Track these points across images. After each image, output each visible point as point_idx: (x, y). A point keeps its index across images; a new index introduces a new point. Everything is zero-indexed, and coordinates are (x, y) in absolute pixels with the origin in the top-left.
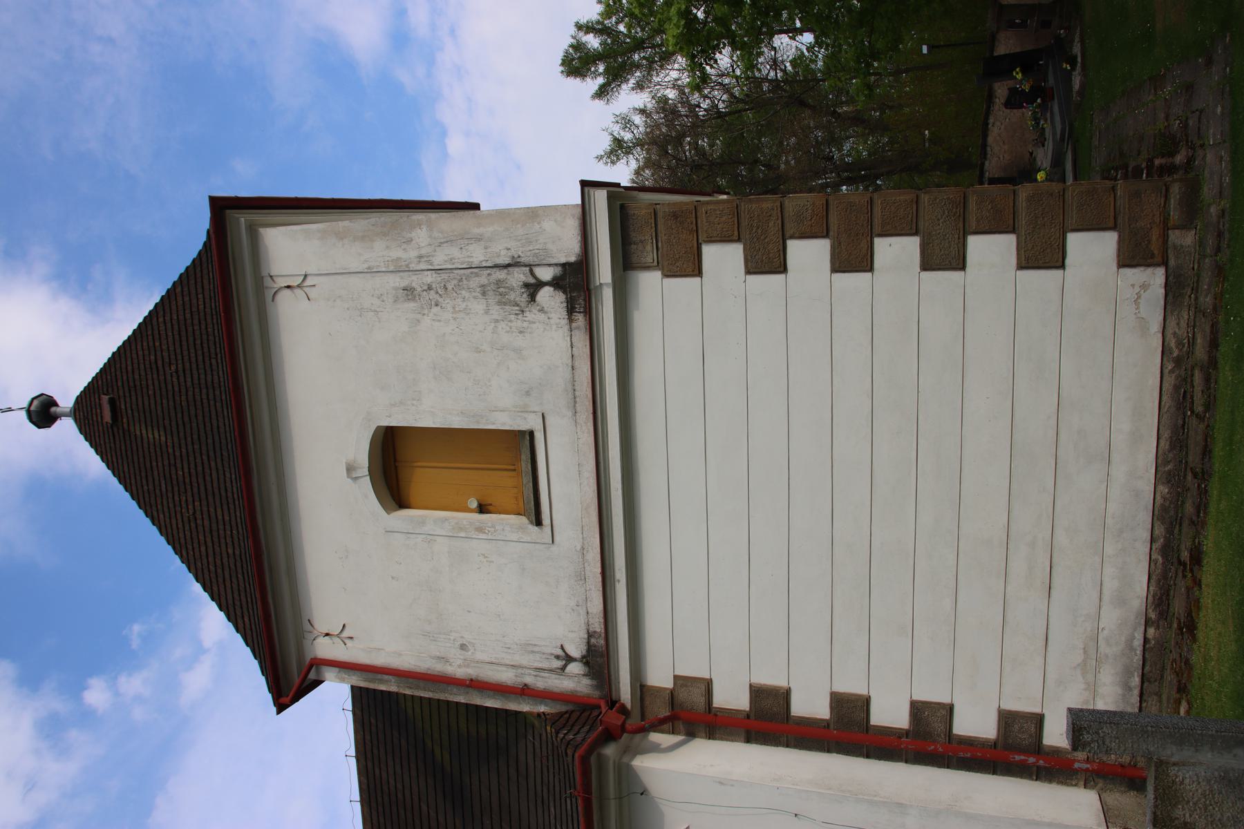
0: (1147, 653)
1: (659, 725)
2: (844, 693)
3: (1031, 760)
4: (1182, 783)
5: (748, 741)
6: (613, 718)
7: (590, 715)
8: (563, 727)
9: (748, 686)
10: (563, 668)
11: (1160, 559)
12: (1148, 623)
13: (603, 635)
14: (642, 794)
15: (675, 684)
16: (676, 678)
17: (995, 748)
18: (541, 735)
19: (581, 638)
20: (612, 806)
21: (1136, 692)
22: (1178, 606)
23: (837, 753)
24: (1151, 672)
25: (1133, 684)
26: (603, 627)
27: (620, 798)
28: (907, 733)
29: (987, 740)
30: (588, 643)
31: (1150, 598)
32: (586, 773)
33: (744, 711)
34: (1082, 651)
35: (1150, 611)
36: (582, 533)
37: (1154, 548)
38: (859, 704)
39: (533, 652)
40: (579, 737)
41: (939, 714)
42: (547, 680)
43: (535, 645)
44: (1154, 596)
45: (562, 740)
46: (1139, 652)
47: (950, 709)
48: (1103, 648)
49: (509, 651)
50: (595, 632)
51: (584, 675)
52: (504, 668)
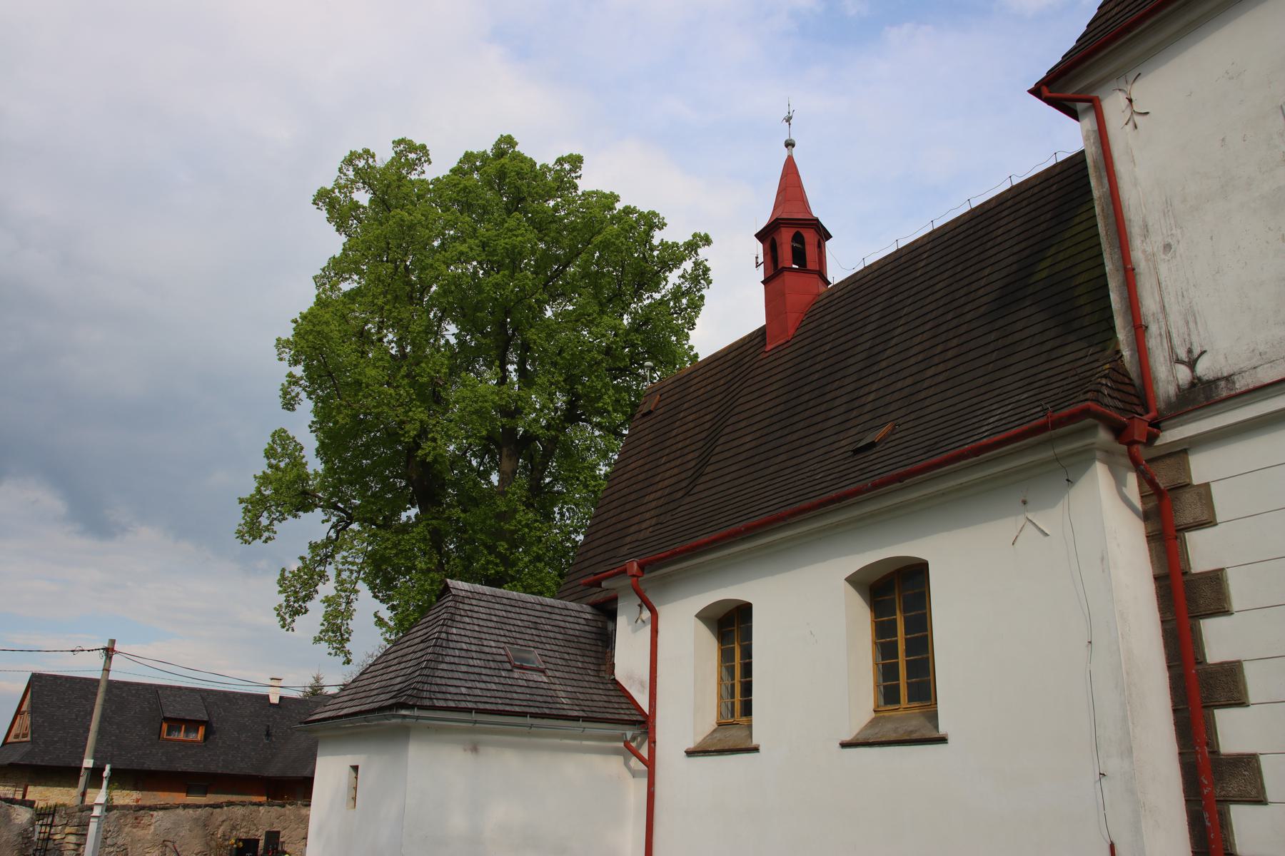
1: (1147, 480)
2: (1244, 676)
5: (1157, 578)
6: (1139, 430)
10: (1179, 361)
13: (1233, 393)
14: (1068, 480)
16: (1207, 486)
18: (1097, 360)
26: (1243, 389)
28: (1215, 752)
32: (1072, 418)
33: (1190, 568)
39: (1187, 323)
40: (1107, 400)
43: (1196, 323)
45: (1099, 383)
49: (1180, 298)
50: (1234, 383)
51: (1178, 386)
52: (1158, 299)
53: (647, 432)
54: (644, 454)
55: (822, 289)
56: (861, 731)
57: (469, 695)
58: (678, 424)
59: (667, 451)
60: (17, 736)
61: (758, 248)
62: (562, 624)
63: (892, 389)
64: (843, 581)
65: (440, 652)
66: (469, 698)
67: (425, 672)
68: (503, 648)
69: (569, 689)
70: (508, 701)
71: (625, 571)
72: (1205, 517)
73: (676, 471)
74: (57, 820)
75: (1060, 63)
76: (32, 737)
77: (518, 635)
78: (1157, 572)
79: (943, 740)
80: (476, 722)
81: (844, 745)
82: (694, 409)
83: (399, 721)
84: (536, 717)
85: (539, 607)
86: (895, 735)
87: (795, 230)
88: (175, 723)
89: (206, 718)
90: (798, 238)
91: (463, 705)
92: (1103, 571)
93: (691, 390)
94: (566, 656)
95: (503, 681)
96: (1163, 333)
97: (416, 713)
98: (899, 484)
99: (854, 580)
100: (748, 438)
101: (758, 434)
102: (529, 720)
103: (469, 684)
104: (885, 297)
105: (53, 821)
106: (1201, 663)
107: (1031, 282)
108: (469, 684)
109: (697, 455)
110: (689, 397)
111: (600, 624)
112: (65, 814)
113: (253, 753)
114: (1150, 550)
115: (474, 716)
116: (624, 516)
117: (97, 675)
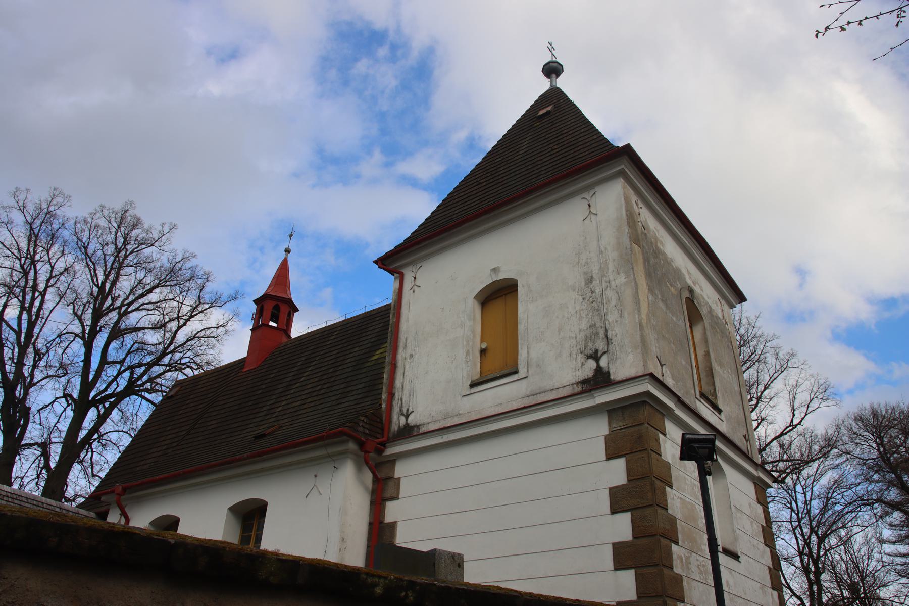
5: (370, 524)
7: (379, 433)
10: (402, 414)
14: (335, 467)
16: (399, 479)
27: (330, 456)
30: (415, 426)
33: (384, 520)
40: (361, 429)
50: (420, 429)
52: (402, 381)
55: (285, 340)
61: (254, 308)
71: (113, 492)
72: (394, 495)
75: (393, 250)
87: (276, 303)
90: (277, 308)
100: (214, 422)
107: (370, 360)
114: (371, 509)
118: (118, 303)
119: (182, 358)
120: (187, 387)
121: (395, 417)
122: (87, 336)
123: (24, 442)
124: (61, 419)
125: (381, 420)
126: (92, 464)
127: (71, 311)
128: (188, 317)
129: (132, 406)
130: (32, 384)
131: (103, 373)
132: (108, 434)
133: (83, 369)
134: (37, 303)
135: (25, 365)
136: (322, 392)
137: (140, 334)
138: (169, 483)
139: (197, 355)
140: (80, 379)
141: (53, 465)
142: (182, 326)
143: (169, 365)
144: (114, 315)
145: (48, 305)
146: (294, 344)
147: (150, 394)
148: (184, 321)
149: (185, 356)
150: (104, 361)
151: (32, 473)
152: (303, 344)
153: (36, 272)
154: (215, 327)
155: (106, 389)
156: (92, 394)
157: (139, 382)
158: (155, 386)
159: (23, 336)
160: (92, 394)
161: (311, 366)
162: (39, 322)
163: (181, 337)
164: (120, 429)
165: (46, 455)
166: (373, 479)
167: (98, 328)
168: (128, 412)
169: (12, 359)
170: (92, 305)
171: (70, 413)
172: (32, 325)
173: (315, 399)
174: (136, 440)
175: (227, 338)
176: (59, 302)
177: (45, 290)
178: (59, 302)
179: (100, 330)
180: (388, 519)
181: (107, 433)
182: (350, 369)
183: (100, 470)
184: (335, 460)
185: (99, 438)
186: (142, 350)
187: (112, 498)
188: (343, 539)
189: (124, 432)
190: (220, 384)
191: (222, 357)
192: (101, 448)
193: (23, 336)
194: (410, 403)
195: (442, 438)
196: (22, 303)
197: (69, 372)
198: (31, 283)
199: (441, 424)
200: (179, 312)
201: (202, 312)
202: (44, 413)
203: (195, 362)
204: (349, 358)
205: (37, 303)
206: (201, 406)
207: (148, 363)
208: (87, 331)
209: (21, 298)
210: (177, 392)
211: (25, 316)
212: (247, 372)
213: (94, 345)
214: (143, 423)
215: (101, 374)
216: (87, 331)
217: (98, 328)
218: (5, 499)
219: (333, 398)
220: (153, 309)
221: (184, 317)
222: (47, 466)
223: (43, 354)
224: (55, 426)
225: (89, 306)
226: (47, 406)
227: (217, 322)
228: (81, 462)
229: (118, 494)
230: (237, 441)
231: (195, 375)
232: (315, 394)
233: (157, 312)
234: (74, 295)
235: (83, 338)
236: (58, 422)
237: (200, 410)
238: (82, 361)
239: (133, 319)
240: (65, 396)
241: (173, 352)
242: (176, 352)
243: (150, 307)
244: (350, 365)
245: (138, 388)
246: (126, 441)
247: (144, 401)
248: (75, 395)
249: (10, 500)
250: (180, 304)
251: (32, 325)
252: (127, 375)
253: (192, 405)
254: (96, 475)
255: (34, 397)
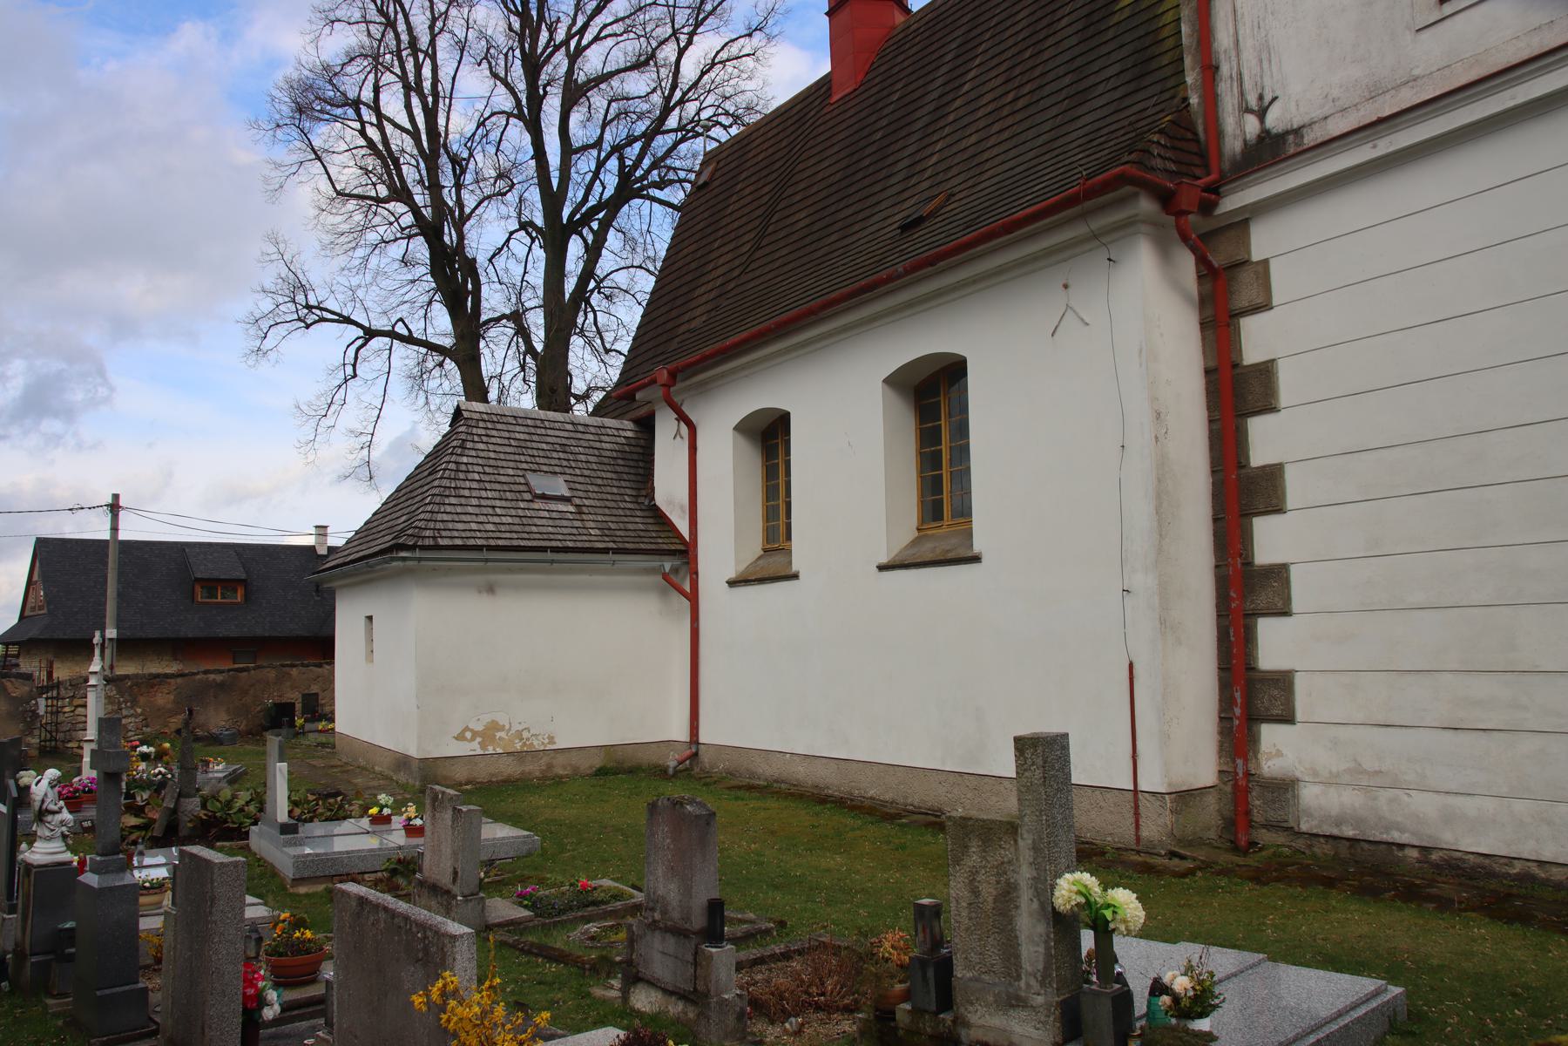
0: (1384, 846)
1: (1202, 261)
2: (1284, 480)
3: (1238, 711)
4: (1000, 846)
5: (1208, 372)
6: (1189, 197)
7: (1196, 166)
8: (1170, 138)
9: (1273, 357)
10: (1248, 110)
11: (1515, 871)
12: (1425, 850)
13: (1300, 149)
14: (1109, 260)
15: (1258, 263)
16: (1265, 262)
17: (1247, 669)
18: (1162, 111)
19: (1291, 120)
20: (1080, 230)
21: (1335, 832)
22: (1446, 889)
23: (1213, 483)
24: (1362, 849)
25: (1344, 828)
26: (1312, 144)
27: (1095, 236)
28: (1249, 563)
29: (1255, 659)
30: (1287, 133)
31: (1458, 855)
32: (1107, 186)
33: (1242, 360)
34: (1377, 769)
35: (1441, 854)
36: (1439, 70)
37: (1529, 864)
38: (1274, 501)
39: (1261, 61)
40: (1158, 163)
41: (1276, 599)
42: (1229, 94)
43: (1270, 61)
44: (1460, 859)
45: (1150, 141)
46: (1385, 837)
47: (1285, 612)
48: (1384, 795)
49: (1256, 29)
50: (1302, 137)
51: (1245, 141)
52: (1231, 31)
53: (701, 209)
54: (696, 237)
55: (900, 18)
56: (901, 552)
57: (479, 531)
58: (734, 198)
59: (721, 233)
60: (33, 609)
62: (598, 445)
63: (955, 149)
64: (878, 386)
65: (448, 485)
66: (479, 534)
67: (429, 508)
68: (523, 476)
69: (599, 518)
70: (526, 536)
71: (654, 382)
73: (729, 256)
74: (63, 692)
76: (48, 610)
77: (542, 461)
78: (1212, 364)
79: (976, 559)
80: (487, 560)
81: (882, 568)
82: (754, 179)
83: (400, 564)
84: (558, 552)
85: (569, 427)
86: (931, 555)
88: (211, 585)
89: (243, 576)
91: (471, 542)
92: (1141, 365)
93: (751, 155)
94: (599, 482)
95: (521, 513)
96: (1234, 75)
97: (418, 554)
98: (930, 269)
99: (892, 381)
100: (803, 214)
101: (812, 210)
102: (549, 555)
103: (482, 519)
104: (963, 30)
105: (58, 694)
106: (1244, 467)
108: (482, 519)
109: (753, 235)
110: (748, 164)
111: (642, 442)
112: (71, 685)
113: (303, 612)
114: (1204, 339)
115: (486, 554)
116: (674, 313)
117: (106, 536)
118: (560, 35)
119: (700, 109)
120: (729, 159)
121: (1229, 121)
122: (526, 110)
123: (484, 318)
124: (529, 267)
125: (1196, 134)
126: (599, 332)
127: (487, 73)
128: (691, 28)
129: (638, 217)
130: (464, 219)
131: (573, 170)
132: (611, 276)
133: (537, 170)
134: (427, 72)
135: (444, 187)
136: (1020, 104)
137: (615, 82)
138: (767, 343)
139: (727, 98)
140: (538, 190)
141: (539, 347)
142: (686, 48)
143: (681, 128)
144: (560, 60)
145: (445, 73)
146: (923, 21)
147: (662, 189)
148: (687, 36)
149: (704, 105)
150: (568, 150)
151: (512, 366)
152: (945, 15)
153: (406, 16)
154: (745, 36)
155: (585, 199)
156: (566, 213)
157: (639, 173)
158: (665, 175)
159: (424, 137)
160: (566, 213)
161: (977, 56)
162: (441, 105)
163: (689, 71)
164: (628, 263)
165: (523, 332)
166: (1198, 271)
167: (541, 92)
168: (633, 231)
169: (421, 182)
170: (517, 53)
171: (539, 253)
172: (431, 114)
173: (1009, 121)
174: (663, 278)
175: (772, 50)
176: (461, 58)
177: (432, 43)
178: (461, 58)
179: (546, 93)
180: (1252, 355)
181: (608, 275)
182: (1074, 40)
183: (616, 339)
184: (1108, 240)
185: (598, 287)
186: (626, 113)
187: (656, 392)
188: (1159, 414)
189: (637, 267)
190: (792, 138)
191: (769, 92)
192: (605, 301)
193: (424, 137)
194: (1265, 79)
195: (1375, 147)
196: (403, 77)
197: (515, 181)
198: (404, 37)
199: (1362, 113)
200: (673, 22)
201: (710, 13)
202: (500, 262)
203: (727, 113)
204: (1063, 17)
205: (427, 72)
206: (766, 189)
207: (644, 135)
208: (524, 102)
209: (397, 70)
210: (713, 174)
211: (415, 101)
212: (840, 103)
213: (543, 125)
214: (666, 246)
215: (570, 174)
216: (524, 102)
217: (541, 92)
218: (481, 424)
219: (1054, 111)
220: (624, 32)
221: (686, 30)
222: (530, 349)
223: (464, 159)
224: (523, 280)
225: (514, 56)
226: (500, 249)
227: (747, 23)
228: (582, 333)
229: (663, 385)
230: (862, 241)
231: (732, 138)
232: (1005, 112)
233: (632, 35)
234: (484, 43)
235: (520, 117)
236: (525, 272)
237: (767, 197)
238: (532, 158)
239: (593, 61)
240: (525, 226)
241: (682, 102)
242: (688, 101)
243: (618, 28)
244: (1070, 30)
245: (639, 185)
246: (646, 283)
247: (656, 206)
248: (539, 221)
249: (489, 425)
250: (671, 9)
251: (431, 114)
252: (613, 163)
253: (747, 191)
254: (611, 350)
255: (475, 237)
